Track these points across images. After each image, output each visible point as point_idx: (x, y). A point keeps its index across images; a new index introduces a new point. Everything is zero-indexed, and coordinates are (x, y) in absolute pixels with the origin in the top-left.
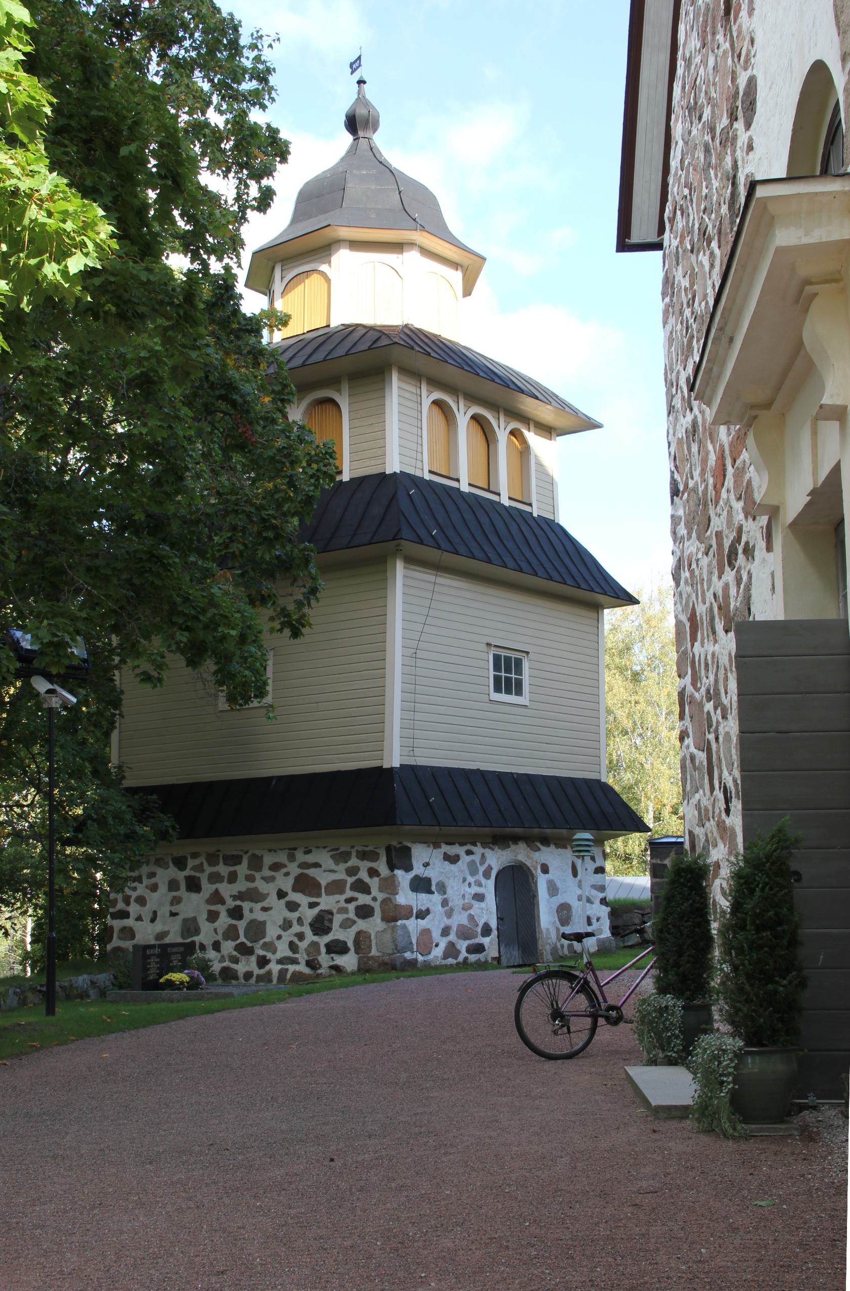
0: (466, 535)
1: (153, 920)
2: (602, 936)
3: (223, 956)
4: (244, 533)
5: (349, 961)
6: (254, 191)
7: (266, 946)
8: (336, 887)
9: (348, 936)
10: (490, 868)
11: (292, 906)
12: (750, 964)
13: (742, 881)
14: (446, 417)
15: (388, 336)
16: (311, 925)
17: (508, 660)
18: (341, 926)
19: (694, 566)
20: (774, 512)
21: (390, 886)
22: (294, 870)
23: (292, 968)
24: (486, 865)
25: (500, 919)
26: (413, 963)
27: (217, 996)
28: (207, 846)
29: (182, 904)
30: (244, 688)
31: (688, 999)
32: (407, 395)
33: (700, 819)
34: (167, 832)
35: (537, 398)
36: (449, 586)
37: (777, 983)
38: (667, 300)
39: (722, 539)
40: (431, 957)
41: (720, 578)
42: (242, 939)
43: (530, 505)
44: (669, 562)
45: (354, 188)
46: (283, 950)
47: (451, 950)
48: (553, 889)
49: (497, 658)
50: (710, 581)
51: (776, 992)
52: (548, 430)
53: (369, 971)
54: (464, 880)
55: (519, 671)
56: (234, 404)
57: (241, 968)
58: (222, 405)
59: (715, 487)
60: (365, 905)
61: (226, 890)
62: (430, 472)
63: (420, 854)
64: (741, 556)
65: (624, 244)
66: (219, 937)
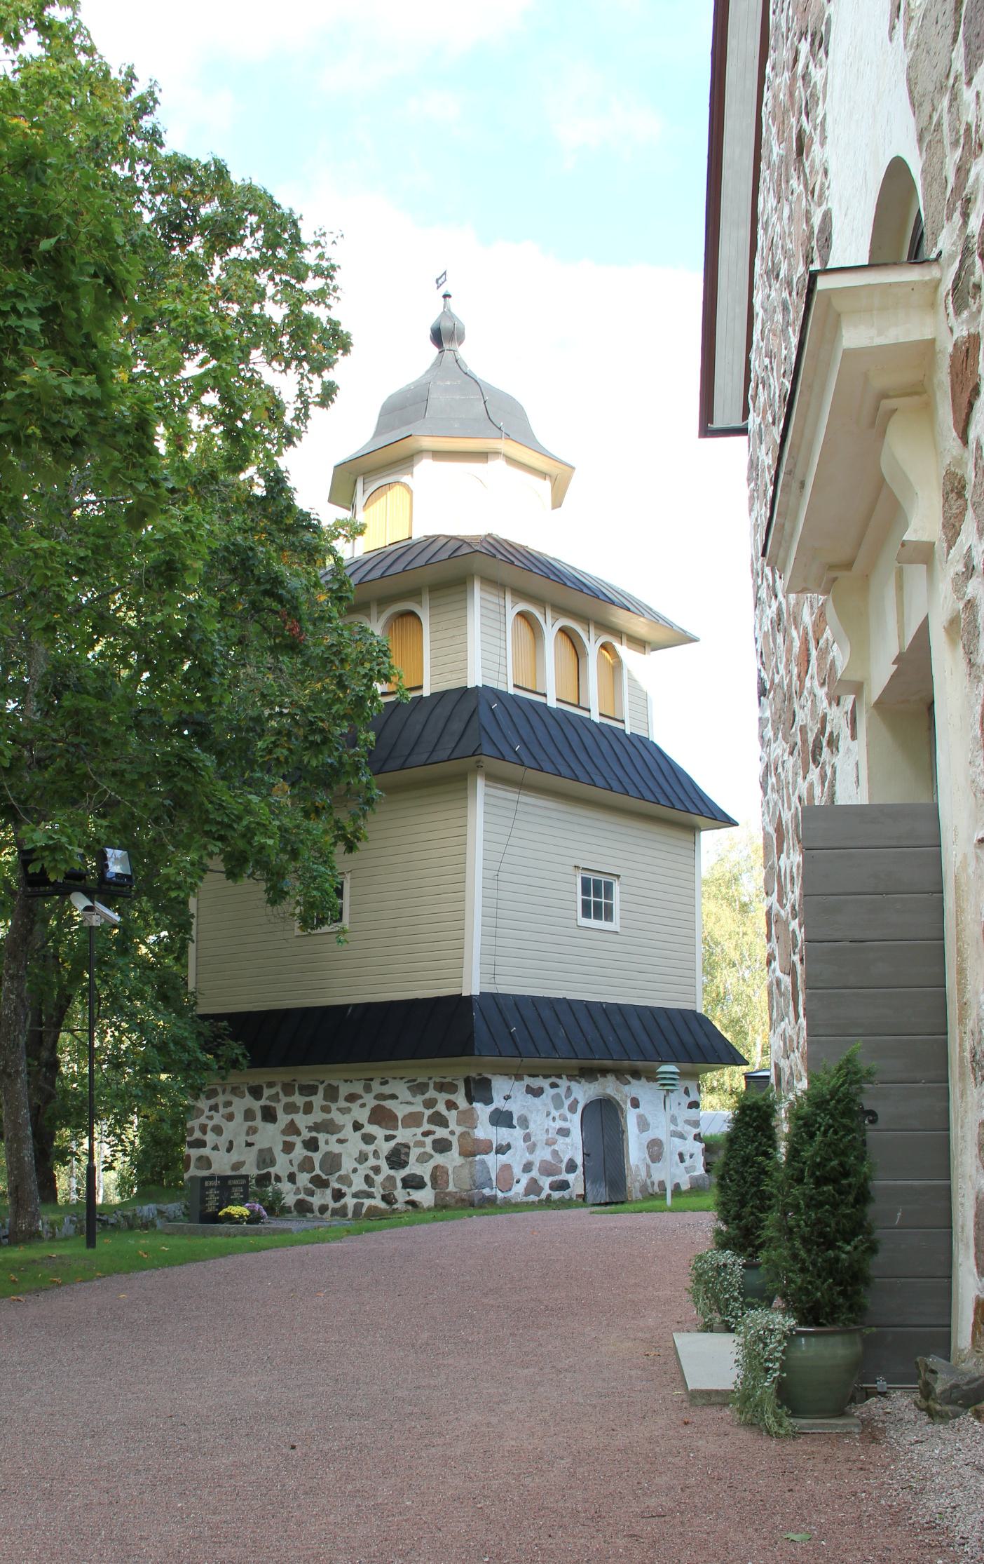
0: (551, 750)
1: (229, 1150)
2: (696, 1174)
4: (289, 738)
5: (425, 1197)
6: (317, 388)
7: (341, 1179)
8: (413, 1120)
9: (425, 1171)
10: (576, 1102)
11: (368, 1139)
12: (807, 1225)
13: (801, 1122)
14: (532, 629)
15: (469, 544)
16: (387, 1158)
17: (597, 883)
18: (417, 1160)
19: (780, 770)
20: (858, 688)
21: (468, 1119)
23: (367, 1202)
24: (572, 1099)
25: (586, 1155)
26: (492, 1200)
27: (275, 1232)
28: (282, 1075)
30: (321, 911)
31: (750, 1256)
32: (492, 606)
33: (785, 1051)
34: (237, 1060)
35: (629, 610)
36: (534, 806)
37: (839, 1248)
38: (752, 485)
39: (806, 733)
40: (511, 1194)
41: (805, 778)
42: (317, 1171)
43: (623, 722)
44: (759, 769)
45: (438, 399)
46: (359, 1184)
47: (533, 1187)
48: (643, 1125)
49: (585, 882)
50: (795, 782)
51: (837, 1259)
52: (641, 644)
53: (445, 1207)
54: (548, 1114)
55: (609, 894)
56: (280, 599)
57: (316, 1201)
58: (268, 601)
59: (799, 676)
61: (302, 1121)
62: (515, 686)
63: (500, 1086)
64: (825, 749)
65: (707, 429)
66: (295, 1169)
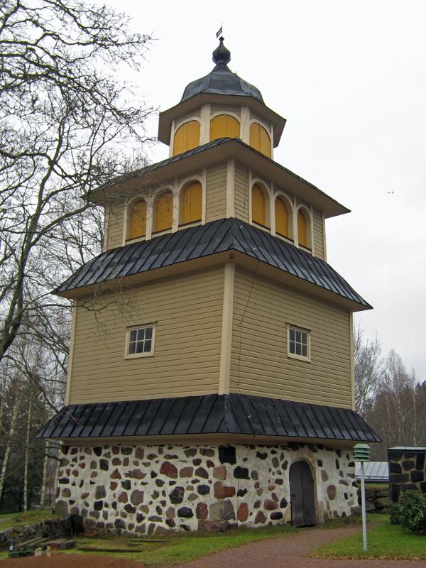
1: (81, 486)
3: (117, 512)
5: (193, 523)
8: (186, 473)
11: (160, 483)
16: (170, 496)
18: (189, 499)
22: (162, 459)
23: (157, 524)
25: (292, 496)
29: (97, 477)
42: (129, 502)
46: (153, 512)
47: (261, 518)
48: (325, 477)
54: (270, 470)
57: (127, 521)
60: (204, 485)
61: (122, 469)
66: (116, 500)
